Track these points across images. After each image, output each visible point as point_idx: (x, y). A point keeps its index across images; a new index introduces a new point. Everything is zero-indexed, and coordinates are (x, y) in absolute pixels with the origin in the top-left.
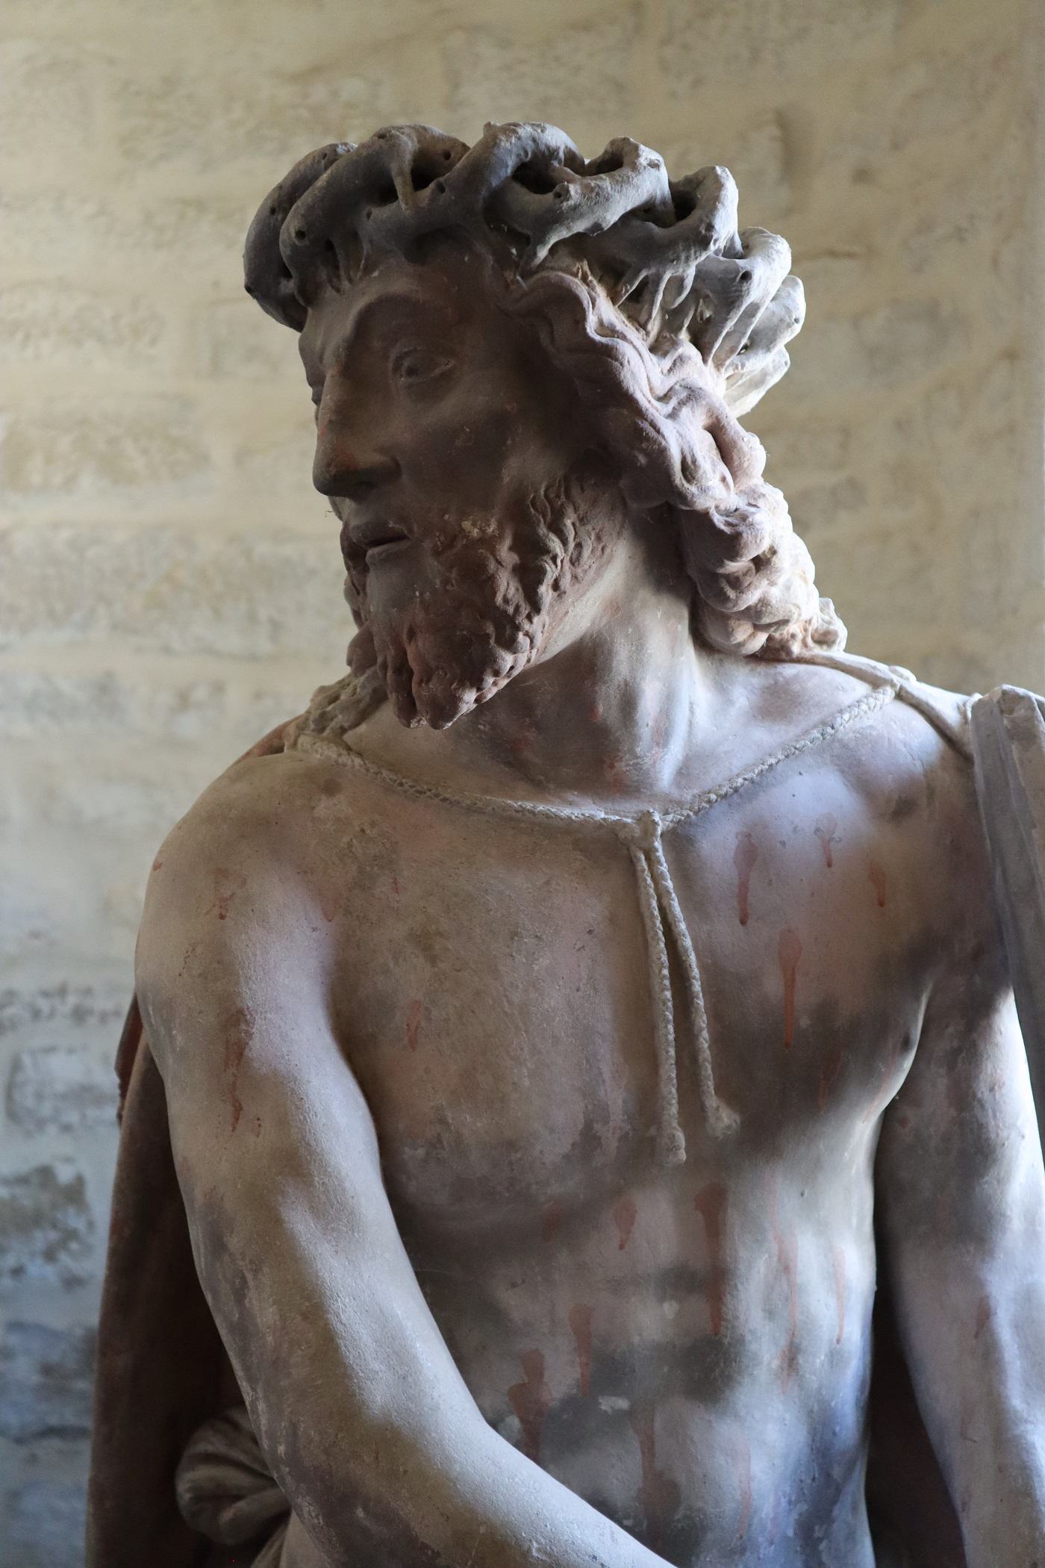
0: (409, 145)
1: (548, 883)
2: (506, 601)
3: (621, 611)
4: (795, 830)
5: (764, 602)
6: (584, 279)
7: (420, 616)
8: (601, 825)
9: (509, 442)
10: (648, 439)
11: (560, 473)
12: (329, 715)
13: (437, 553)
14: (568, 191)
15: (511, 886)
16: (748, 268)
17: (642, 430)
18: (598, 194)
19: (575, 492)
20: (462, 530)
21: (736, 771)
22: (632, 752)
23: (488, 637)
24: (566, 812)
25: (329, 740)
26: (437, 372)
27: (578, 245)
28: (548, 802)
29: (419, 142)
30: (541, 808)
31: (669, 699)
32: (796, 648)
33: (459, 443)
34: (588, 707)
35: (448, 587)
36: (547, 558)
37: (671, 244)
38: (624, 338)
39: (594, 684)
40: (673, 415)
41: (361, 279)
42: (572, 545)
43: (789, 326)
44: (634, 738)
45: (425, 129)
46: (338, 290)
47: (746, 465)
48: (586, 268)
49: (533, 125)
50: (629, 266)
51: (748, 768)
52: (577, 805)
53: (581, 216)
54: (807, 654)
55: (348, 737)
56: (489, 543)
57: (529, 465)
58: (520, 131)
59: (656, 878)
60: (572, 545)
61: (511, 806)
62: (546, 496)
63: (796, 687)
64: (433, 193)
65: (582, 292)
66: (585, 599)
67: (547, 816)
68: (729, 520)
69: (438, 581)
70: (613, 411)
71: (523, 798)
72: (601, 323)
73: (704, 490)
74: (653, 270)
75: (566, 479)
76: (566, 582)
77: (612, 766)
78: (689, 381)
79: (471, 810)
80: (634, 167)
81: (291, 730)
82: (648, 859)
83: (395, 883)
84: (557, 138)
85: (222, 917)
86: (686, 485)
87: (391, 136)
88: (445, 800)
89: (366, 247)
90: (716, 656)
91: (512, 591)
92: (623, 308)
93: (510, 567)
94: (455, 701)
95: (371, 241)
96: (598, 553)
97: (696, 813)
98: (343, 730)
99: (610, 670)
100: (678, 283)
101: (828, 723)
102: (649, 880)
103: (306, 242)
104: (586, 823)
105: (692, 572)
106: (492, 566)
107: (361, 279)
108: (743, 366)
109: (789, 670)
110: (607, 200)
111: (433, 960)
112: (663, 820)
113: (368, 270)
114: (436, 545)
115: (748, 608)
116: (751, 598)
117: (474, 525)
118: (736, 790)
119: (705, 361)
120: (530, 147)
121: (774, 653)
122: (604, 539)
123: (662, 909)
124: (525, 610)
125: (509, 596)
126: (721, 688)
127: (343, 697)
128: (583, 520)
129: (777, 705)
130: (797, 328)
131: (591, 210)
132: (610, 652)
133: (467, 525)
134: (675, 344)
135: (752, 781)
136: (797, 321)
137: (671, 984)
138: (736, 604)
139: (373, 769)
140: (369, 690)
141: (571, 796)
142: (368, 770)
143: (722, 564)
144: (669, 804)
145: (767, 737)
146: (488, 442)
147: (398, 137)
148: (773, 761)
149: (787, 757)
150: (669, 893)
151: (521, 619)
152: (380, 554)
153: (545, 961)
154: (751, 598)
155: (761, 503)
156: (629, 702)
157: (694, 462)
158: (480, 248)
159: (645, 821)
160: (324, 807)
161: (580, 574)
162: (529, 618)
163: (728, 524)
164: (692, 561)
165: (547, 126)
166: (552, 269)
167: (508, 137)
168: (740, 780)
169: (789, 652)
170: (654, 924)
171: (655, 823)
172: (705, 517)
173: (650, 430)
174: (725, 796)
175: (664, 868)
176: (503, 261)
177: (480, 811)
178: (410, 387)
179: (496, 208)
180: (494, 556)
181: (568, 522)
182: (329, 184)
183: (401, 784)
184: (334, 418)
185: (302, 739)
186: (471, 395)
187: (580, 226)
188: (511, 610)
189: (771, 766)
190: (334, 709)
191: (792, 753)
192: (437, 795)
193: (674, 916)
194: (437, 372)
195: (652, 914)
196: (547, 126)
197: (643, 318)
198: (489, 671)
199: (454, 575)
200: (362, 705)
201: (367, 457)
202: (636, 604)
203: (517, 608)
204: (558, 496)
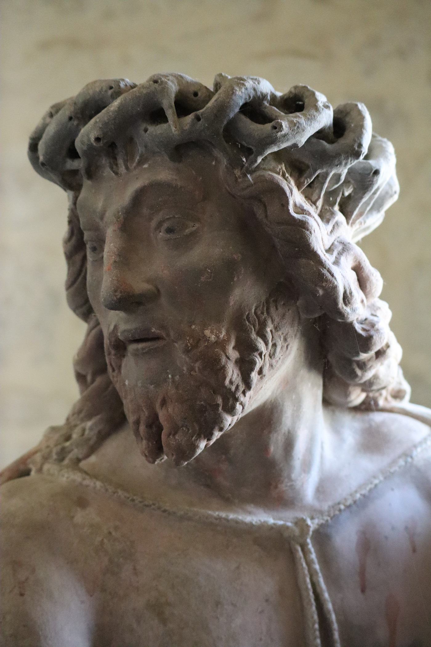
0: (173, 88)
1: (238, 568)
2: (231, 382)
3: (290, 386)
4: (393, 528)
5: (376, 377)
6: (284, 176)
7: (172, 391)
8: (272, 528)
9: (235, 279)
10: (327, 280)
11: (263, 299)
12: (61, 447)
13: (187, 351)
14: (281, 126)
15: (213, 569)
16: (377, 167)
17: (323, 274)
18: (298, 127)
19: (272, 310)
20: (205, 336)
21: (354, 489)
22: (290, 479)
23: (218, 405)
24: (248, 519)
25: (67, 467)
26: (187, 231)
27: (278, 156)
28: (235, 512)
29: (179, 85)
30: (232, 516)
31: (312, 440)
32: (381, 403)
33: (203, 279)
34: (265, 448)
35: (192, 373)
36: (256, 354)
37: (337, 155)
38: (309, 214)
39: (270, 432)
40: (336, 262)
41: (135, 168)
42: (270, 344)
43: (391, 196)
44: (290, 468)
45: (181, 77)
46: (116, 173)
47: (373, 291)
48: (284, 168)
49: (252, 79)
50: (308, 167)
51: (360, 487)
52: (254, 514)
53: (288, 140)
54: (388, 406)
55: (82, 464)
56: (222, 345)
57: (246, 293)
58: (247, 84)
59: (309, 564)
60: (270, 344)
61: (212, 516)
62: (255, 313)
63: (385, 430)
64: (193, 120)
65: (284, 185)
66: (273, 378)
67: (237, 522)
68: (364, 326)
69: (185, 368)
70: (303, 261)
71: (218, 510)
72: (295, 205)
73: (354, 310)
74: (325, 170)
75: (267, 302)
76: (266, 370)
77: (276, 487)
78: (341, 238)
79: (182, 518)
80: (317, 109)
81: (38, 457)
82: (303, 550)
83: (135, 569)
84: (266, 87)
85: (22, 595)
86: (345, 307)
87: (162, 82)
88: (165, 511)
89: (141, 149)
90: (330, 408)
91: (235, 376)
92: (303, 193)
93: (234, 360)
94: (194, 447)
95: (146, 147)
96: (285, 349)
97: (331, 519)
98: (79, 460)
99: (281, 423)
100: (337, 177)
101: (407, 455)
102: (304, 565)
103: (101, 144)
104: (262, 526)
105: (331, 358)
106: (224, 359)
107: (135, 168)
108: (365, 222)
109: (377, 417)
110: (303, 131)
111: (164, 621)
112: (313, 523)
113: (141, 163)
114: (187, 345)
115: (365, 382)
116: (369, 375)
117: (212, 332)
118: (355, 502)
119: (348, 223)
120: (252, 93)
121: (367, 407)
122: (289, 340)
123: (314, 585)
124: (242, 387)
125: (233, 379)
126: (336, 430)
127: (75, 436)
128: (276, 328)
129: (373, 442)
130: (396, 197)
131: (294, 136)
132: (281, 411)
133: (207, 332)
134: (333, 214)
135: (364, 496)
136: (395, 192)
137: (321, 633)
138: (361, 378)
139: (111, 489)
140: (96, 431)
141: (250, 507)
142: (107, 490)
143: (357, 354)
144: (314, 512)
145: (369, 464)
146: (221, 280)
147: (166, 83)
148: (376, 481)
149: (385, 478)
150: (317, 573)
151: (239, 394)
152: (143, 349)
153: (238, 621)
154: (369, 375)
155: (378, 313)
156: (289, 444)
157: (351, 293)
158: (217, 153)
159: (300, 523)
160: (80, 516)
161: (274, 364)
162: (244, 393)
163: (364, 330)
164: (336, 349)
165: (261, 79)
166: (264, 169)
167: (240, 88)
168: (358, 496)
169: (376, 404)
170: (309, 594)
171: (308, 526)
172: (350, 327)
173: (328, 274)
174: (348, 507)
175: (313, 556)
176: (235, 163)
177: (190, 519)
178: (168, 240)
179: (231, 132)
180: (225, 354)
181: (268, 330)
182: (121, 108)
183: (133, 500)
184: (117, 259)
185: (46, 467)
186: (210, 248)
187: (284, 146)
188: (233, 388)
189: (376, 486)
190: (71, 444)
191: (388, 476)
192: (159, 508)
193: (321, 588)
194: (187, 231)
195: (307, 588)
196: (261, 79)
197: (314, 198)
198: (217, 428)
199: (197, 365)
200: (91, 442)
201: (140, 286)
202: (298, 379)
203: (237, 387)
204: (262, 313)
